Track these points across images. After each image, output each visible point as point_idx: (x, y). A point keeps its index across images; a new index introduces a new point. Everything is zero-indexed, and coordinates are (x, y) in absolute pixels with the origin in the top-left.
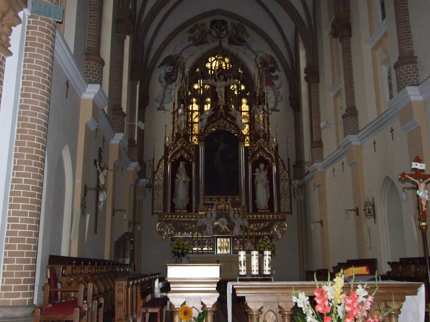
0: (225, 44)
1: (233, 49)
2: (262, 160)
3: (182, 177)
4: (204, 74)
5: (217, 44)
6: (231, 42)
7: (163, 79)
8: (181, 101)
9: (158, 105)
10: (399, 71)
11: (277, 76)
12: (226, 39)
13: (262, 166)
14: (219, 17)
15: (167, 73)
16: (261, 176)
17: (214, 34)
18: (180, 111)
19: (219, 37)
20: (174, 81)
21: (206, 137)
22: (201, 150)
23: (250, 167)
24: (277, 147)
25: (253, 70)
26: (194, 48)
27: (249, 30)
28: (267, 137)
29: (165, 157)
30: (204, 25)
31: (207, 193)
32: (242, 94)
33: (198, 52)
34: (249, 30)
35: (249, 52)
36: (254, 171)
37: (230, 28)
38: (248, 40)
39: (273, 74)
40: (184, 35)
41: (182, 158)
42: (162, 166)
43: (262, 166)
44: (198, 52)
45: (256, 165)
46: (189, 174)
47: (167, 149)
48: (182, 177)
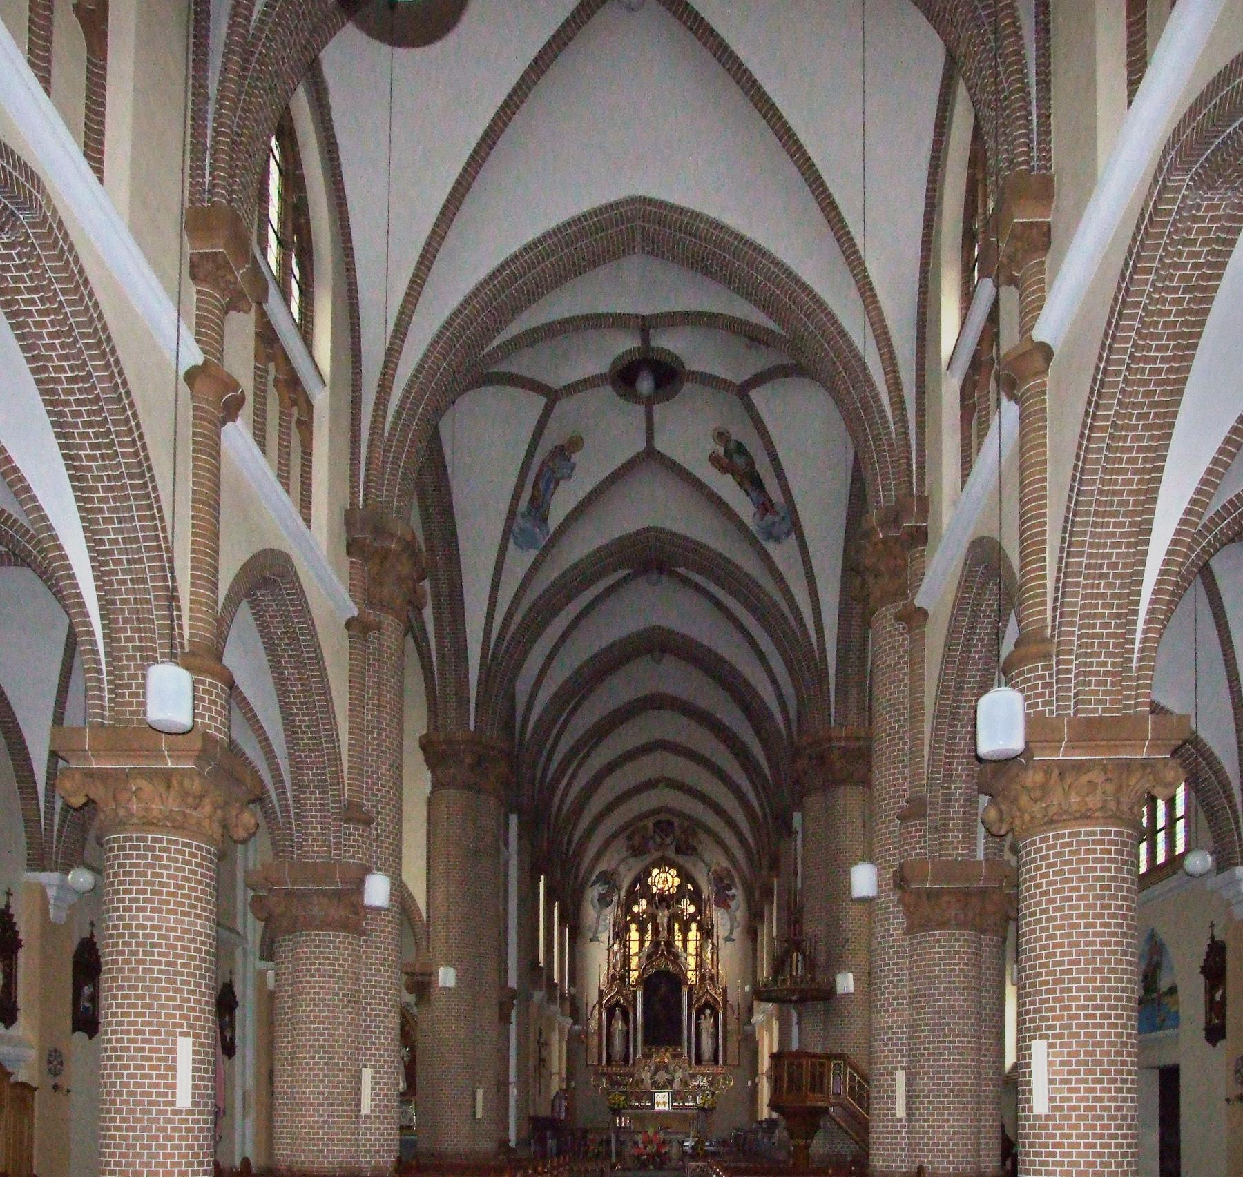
0: (671, 853)
1: (681, 859)
2: (706, 1005)
3: (619, 1025)
4: (646, 893)
5: (659, 854)
6: (678, 850)
7: (596, 902)
8: (616, 935)
9: (591, 935)
10: (906, 827)
11: (734, 896)
12: (673, 848)
13: (708, 1012)
14: (663, 817)
15: (601, 895)
16: (707, 1024)
17: (658, 839)
18: (616, 947)
19: (662, 846)
20: (609, 904)
21: (648, 983)
22: (639, 994)
23: (693, 1015)
24: (725, 990)
25: (707, 889)
26: (632, 860)
27: (702, 836)
28: (713, 979)
29: (600, 1002)
30: (645, 828)
31: (645, 1042)
32: (693, 917)
33: (637, 866)
34: (702, 836)
35: (701, 864)
36: (698, 1018)
37: (678, 831)
38: (700, 848)
39: (729, 893)
40: (620, 844)
41: (618, 1004)
42: (596, 1012)
43: (708, 1012)
44: (637, 866)
45: (700, 1012)
46: (626, 1021)
47: (601, 993)
48: (619, 1025)
